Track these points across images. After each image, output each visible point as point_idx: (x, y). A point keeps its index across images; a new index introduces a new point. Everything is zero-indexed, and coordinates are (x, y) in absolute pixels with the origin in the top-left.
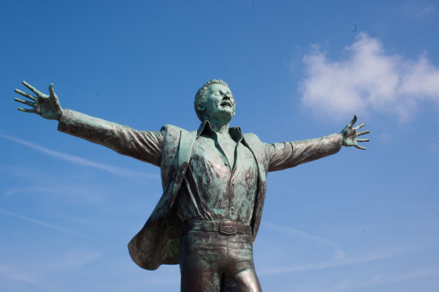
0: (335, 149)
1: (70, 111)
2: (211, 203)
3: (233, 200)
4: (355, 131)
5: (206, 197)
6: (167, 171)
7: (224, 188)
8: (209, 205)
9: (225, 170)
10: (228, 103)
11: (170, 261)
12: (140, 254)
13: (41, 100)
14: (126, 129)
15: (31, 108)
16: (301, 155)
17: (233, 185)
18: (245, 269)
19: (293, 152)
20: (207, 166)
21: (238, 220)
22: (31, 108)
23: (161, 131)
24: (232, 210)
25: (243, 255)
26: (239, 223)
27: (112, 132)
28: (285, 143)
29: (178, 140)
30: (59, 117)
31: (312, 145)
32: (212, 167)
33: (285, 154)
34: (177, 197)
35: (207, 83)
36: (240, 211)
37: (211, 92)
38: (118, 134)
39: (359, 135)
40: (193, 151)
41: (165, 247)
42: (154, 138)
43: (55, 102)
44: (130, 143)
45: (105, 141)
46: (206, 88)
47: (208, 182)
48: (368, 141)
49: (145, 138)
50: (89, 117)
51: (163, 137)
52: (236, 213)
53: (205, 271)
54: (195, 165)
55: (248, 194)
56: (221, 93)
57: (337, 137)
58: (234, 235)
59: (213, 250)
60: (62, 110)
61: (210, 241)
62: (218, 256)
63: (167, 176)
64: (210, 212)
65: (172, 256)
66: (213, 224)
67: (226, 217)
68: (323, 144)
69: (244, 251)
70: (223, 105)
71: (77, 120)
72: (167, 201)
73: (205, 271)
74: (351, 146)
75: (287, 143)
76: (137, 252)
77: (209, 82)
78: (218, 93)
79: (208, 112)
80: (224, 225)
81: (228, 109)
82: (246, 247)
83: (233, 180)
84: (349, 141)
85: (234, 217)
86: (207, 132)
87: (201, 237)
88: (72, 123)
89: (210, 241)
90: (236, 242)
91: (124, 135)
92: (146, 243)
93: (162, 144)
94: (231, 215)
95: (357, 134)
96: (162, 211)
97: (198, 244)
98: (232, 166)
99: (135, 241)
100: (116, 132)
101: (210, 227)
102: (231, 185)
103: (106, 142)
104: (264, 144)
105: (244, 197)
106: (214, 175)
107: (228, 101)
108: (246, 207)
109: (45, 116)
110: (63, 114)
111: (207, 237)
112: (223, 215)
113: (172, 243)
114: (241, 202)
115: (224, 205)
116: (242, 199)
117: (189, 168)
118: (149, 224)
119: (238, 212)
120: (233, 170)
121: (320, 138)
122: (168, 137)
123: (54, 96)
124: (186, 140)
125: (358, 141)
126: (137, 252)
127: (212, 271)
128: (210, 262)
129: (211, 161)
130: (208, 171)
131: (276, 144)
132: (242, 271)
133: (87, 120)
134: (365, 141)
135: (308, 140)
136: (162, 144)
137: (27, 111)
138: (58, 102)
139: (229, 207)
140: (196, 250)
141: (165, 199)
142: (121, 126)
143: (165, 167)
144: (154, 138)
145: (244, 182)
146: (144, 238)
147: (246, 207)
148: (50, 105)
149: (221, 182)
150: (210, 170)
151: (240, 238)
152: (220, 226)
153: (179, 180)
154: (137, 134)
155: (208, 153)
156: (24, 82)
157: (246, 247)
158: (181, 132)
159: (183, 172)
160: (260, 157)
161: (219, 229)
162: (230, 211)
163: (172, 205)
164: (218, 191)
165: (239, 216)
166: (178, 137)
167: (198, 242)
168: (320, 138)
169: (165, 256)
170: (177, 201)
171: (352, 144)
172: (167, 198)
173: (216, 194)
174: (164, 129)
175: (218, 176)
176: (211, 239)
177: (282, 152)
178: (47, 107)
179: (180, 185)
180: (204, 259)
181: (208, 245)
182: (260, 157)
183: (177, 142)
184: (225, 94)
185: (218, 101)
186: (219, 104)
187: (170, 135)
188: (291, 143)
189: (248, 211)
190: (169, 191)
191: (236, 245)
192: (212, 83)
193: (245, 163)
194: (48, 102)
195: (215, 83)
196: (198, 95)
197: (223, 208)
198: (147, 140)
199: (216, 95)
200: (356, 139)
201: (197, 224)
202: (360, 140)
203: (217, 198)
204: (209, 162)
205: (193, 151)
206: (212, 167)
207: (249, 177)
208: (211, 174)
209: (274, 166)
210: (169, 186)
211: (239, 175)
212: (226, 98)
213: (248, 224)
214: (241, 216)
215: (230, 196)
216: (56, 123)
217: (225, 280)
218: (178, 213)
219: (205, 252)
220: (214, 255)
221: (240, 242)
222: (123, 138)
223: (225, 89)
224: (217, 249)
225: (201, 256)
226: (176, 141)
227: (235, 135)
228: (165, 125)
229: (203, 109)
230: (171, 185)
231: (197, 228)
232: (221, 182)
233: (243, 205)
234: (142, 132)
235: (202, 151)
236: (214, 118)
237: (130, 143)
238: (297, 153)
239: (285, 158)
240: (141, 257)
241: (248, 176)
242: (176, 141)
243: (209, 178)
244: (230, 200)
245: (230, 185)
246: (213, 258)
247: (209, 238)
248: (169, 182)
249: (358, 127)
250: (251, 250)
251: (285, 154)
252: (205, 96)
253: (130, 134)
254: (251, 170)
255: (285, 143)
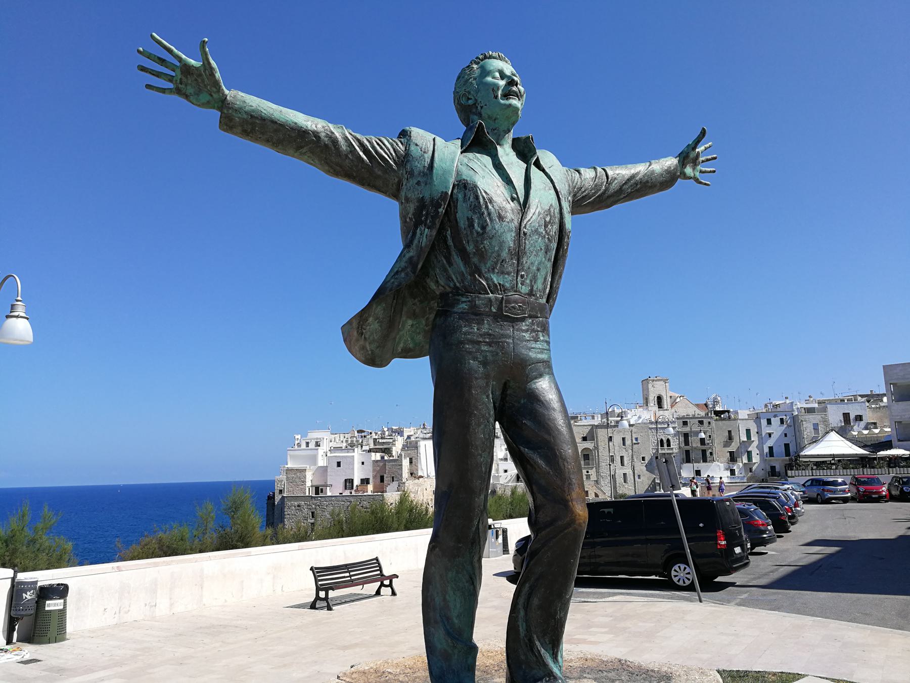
0: (669, 180)
1: (240, 93)
2: (488, 265)
3: (525, 260)
4: (698, 155)
5: (482, 255)
6: (412, 208)
7: (509, 239)
8: (484, 270)
9: (510, 207)
10: (515, 92)
11: (408, 353)
12: (362, 342)
13: (187, 69)
14: (340, 130)
15: (171, 85)
16: (620, 190)
17: (525, 234)
18: (541, 376)
19: (609, 183)
20: (481, 201)
21: (531, 293)
22: (171, 85)
23: (399, 137)
24: (522, 276)
25: (539, 353)
26: (532, 299)
27: (316, 134)
28: (595, 168)
29: (430, 153)
30: (222, 104)
31: (638, 173)
32: (491, 202)
33: (597, 187)
34: (429, 253)
35: (477, 58)
36: (534, 279)
37: (485, 72)
38: (326, 139)
39: (703, 162)
40: (458, 173)
41: (401, 333)
42: (388, 150)
43: (212, 75)
44: (346, 156)
45: (304, 150)
46: (475, 66)
47: (484, 228)
48: (714, 172)
49: (373, 147)
50: (274, 106)
51: (403, 148)
52: (528, 281)
53: (477, 379)
54: (460, 196)
55: (547, 250)
56: (503, 76)
57: (671, 162)
58: (523, 319)
59: (489, 344)
60: (227, 92)
61: (485, 328)
62: (497, 354)
63: (410, 215)
64: (486, 280)
65: (411, 346)
66: (490, 300)
67: (512, 288)
68: (653, 172)
69: (538, 345)
70: (507, 95)
71: (253, 111)
72: (411, 258)
73: (477, 379)
74: (690, 178)
75: (599, 169)
76: (357, 340)
77: (481, 57)
78: (497, 75)
79: (479, 108)
80: (508, 302)
81: (515, 102)
82: (542, 338)
83: (525, 227)
84: (689, 170)
85: (525, 289)
86: (478, 142)
87: (469, 322)
88: (245, 116)
89: (485, 328)
90: (527, 331)
91: (338, 141)
92: (373, 326)
93: (404, 159)
94: (520, 285)
95: (701, 159)
96: (403, 275)
97: (465, 334)
98: (522, 200)
99: (355, 324)
100: (322, 135)
101: (486, 305)
102: (522, 235)
103: (305, 154)
104: (565, 168)
105: (541, 254)
106: (495, 216)
107: (514, 88)
108: (543, 272)
109: (194, 101)
110: (228, 98)
111: (480, 323)
112: (507, 285)
113: (412, 326)
114: (536, 263)
115: (510, 269)
116: (537, 259)
117: (452, 202)
118: (379, 295)
119: (531, 281)
120: (524, 206)
121: (648, 164)
122: (413, 148)
123: (209, 63)
124: (447, 154)
125: (701, 172)
126: (357, 340)
127: (487, 377)
128: (485, 363)
129: (488, 191)
130: (484, 210)
131: (582, 170)
132: (536, 378)
133: (271, 112)
134: (710, 172)
135: (629, 166)
136: (404, 159)
137: (163, 91)
138: (218, 75)
139: (518, 271)
140: (462, 343)
141: (408, 256)
142: (331, 127)
143: (407, 200)
144: (387, 147)
145: (542, 230)
146: (371, 319)
147: (543, 272)
148: (203, 81)
149: (506, 229)
150: (487, 207)
151: (533, 324)
152: (501, 302)
153: (433, 223)
154: (359, 140)
155: (483, 177)
156: (154, 34)
157: (542, 338)
158: (434, 139)
159: (440, 210)
160: (563, 188)
161: (500, 308)
162: (519, 278)
163: (420, 266)
164: (501, 244)
165: (532, 287)
166: (431, 149)
167: (464, 329)
168: (648, 164)
169: (401, 345)
170: (428, 259)
171: (692, 175)
172: (412, 253)
173: (496, 249)
174: (404, 134)
175: (501, 218)
176: (486, 326)
177: (592, 183)
178: (195, 84)
179: (434, 233)
180: (475, 359)
181: (481, 335)
182: (563, 188)
183: (428, 157)
184: (509, 77)
185: (498, 89)
186: (500, 93)
187: (417, 145)
188: (604, 170)
189: (545, 279)
190: (416, 242)
191: (527, 336)
192: (485, 57)
193: (542, 198)
194: (200, 75)
195: (491, 57)
196: (463, 78)
197: (508, 273)
198: (376, 152)
199: (494, 78)
200: (699, 168)
201: (464, 299)
202: (704, 169)
203: (499, 255)
204: (486, 192)
205: (458, 173)
206: (491, 202)
207: (550, 222)
208: (489, 214)
209: (584, 202)
210: (414, 234)
211: (534, 217)
212: (511, 83)
213: (544, 301)
214: (535, 289)
215: (518, 253)
216: (215, 115)
217: (508, 392)
218: (428, 281)
219: (477, 346)
220: (491, 352)
221: (533, 331)
222: (335, 146)
223: (508, 69)
224: (495, 341)
225: (470, 353)
226: (426, 155)
227: (524, 150)
228: (408, 128)
229: (470, 102)
230: (418, 231)
231: (464, 306)
232: (506, 229)
233: (538, 270)
234: (368, 137)
235: (472, 172)
236: (489, 117)
237: (346, 156)
238: (614, 186)
239: (596, 193)
240: (363, 348)
241: (548, 219)
242: (426, 155)
243: (486, 221)
244: (518, 260)
245: (520, 233)
246: (490, 357)
247: (483, 324)
248: (416, 226)
249: (703, 148)
250: (548, 343)
251: (596, 186)
252: (475, 79)
253: (346, 139)
254: (552, 210)
255: (595, 168)
